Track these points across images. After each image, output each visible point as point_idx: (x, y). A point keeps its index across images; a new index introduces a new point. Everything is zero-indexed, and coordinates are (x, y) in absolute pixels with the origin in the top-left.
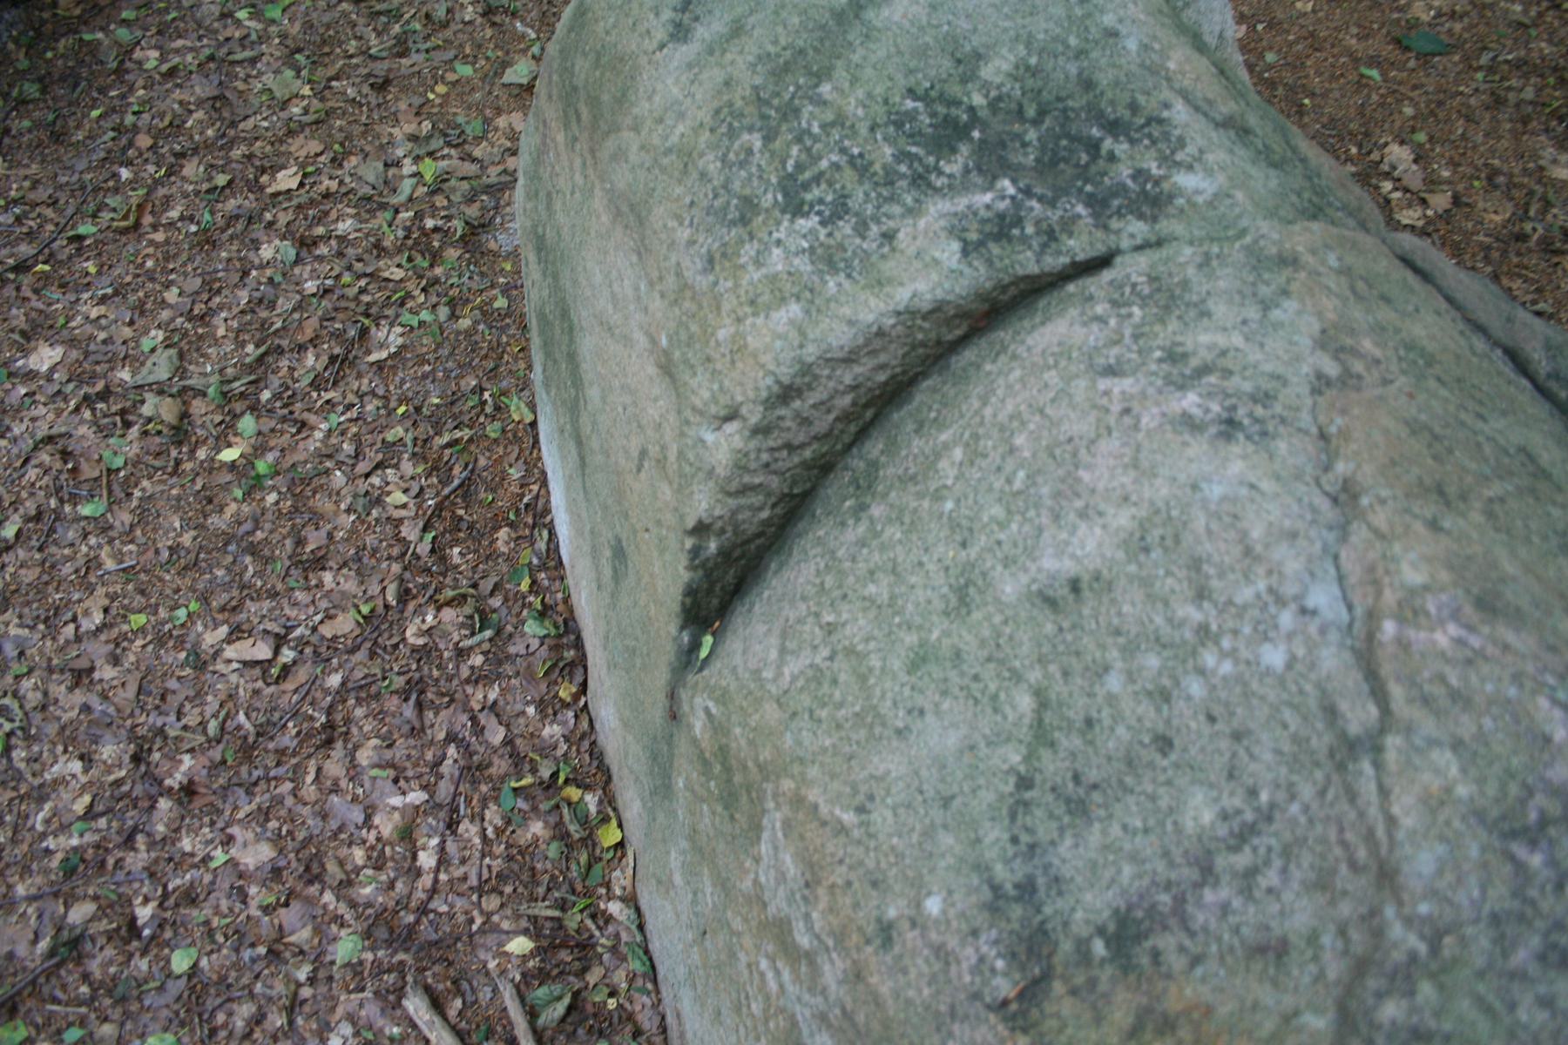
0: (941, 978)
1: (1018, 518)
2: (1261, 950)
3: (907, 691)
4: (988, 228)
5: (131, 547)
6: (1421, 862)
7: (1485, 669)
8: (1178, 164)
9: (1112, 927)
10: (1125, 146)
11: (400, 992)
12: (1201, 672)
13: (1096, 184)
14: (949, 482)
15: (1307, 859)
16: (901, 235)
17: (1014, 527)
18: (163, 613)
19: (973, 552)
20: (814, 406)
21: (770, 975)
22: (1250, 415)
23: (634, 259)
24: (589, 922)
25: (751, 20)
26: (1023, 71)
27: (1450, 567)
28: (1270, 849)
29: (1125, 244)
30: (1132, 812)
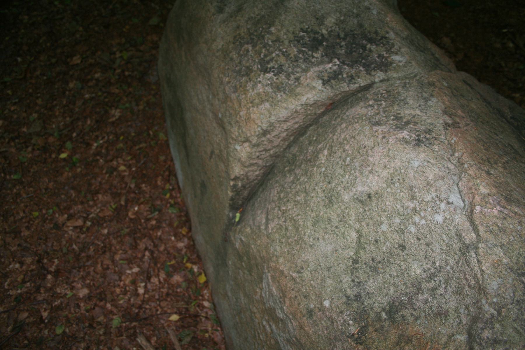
0: (331, 328)
1: (348, 173)
2: (440, 314)
3: (312, 232)
4: (331, 75)
5: (31, 189)
6: (493, 285)
7: (510, 220)
8: (393, 52)
9: (388, 308)
10: (374, 47)
11: (135, 335)
12: (414, 224)
13: (366, 60)
14: (323, 162)
15: (453, 284)
16: (302, 79)
17: (347, 176)
18: (44, 212)
19: (333, 185)
20: (274, 137)
21: (267, 327)
22: (425, 137)
23: (207, 87)
24: (197, 308)
25: (245, 5)
26: (339, 22)
27: (495, 187)
28: (440, 281)
29: (377, 80)
30: (393, 270)
